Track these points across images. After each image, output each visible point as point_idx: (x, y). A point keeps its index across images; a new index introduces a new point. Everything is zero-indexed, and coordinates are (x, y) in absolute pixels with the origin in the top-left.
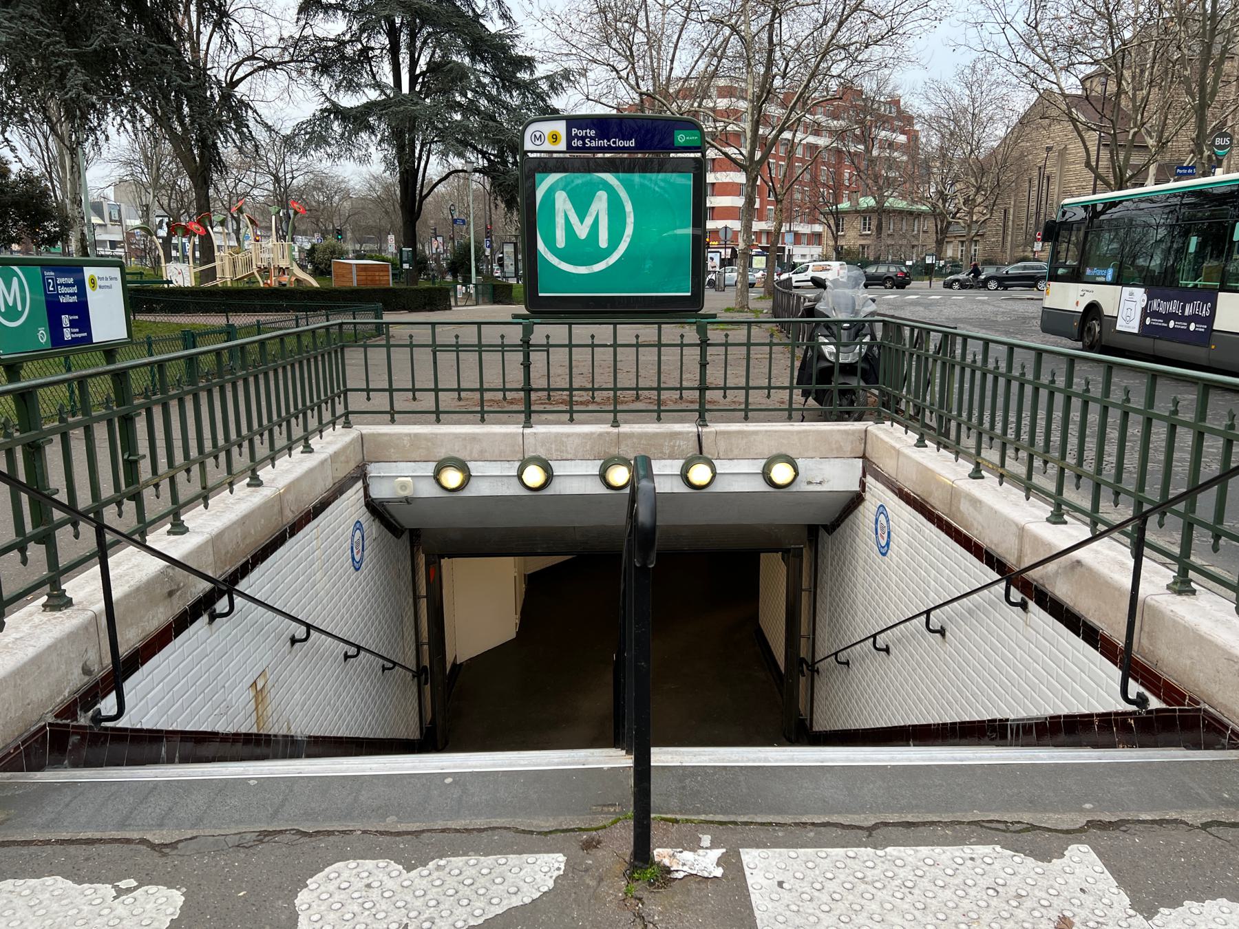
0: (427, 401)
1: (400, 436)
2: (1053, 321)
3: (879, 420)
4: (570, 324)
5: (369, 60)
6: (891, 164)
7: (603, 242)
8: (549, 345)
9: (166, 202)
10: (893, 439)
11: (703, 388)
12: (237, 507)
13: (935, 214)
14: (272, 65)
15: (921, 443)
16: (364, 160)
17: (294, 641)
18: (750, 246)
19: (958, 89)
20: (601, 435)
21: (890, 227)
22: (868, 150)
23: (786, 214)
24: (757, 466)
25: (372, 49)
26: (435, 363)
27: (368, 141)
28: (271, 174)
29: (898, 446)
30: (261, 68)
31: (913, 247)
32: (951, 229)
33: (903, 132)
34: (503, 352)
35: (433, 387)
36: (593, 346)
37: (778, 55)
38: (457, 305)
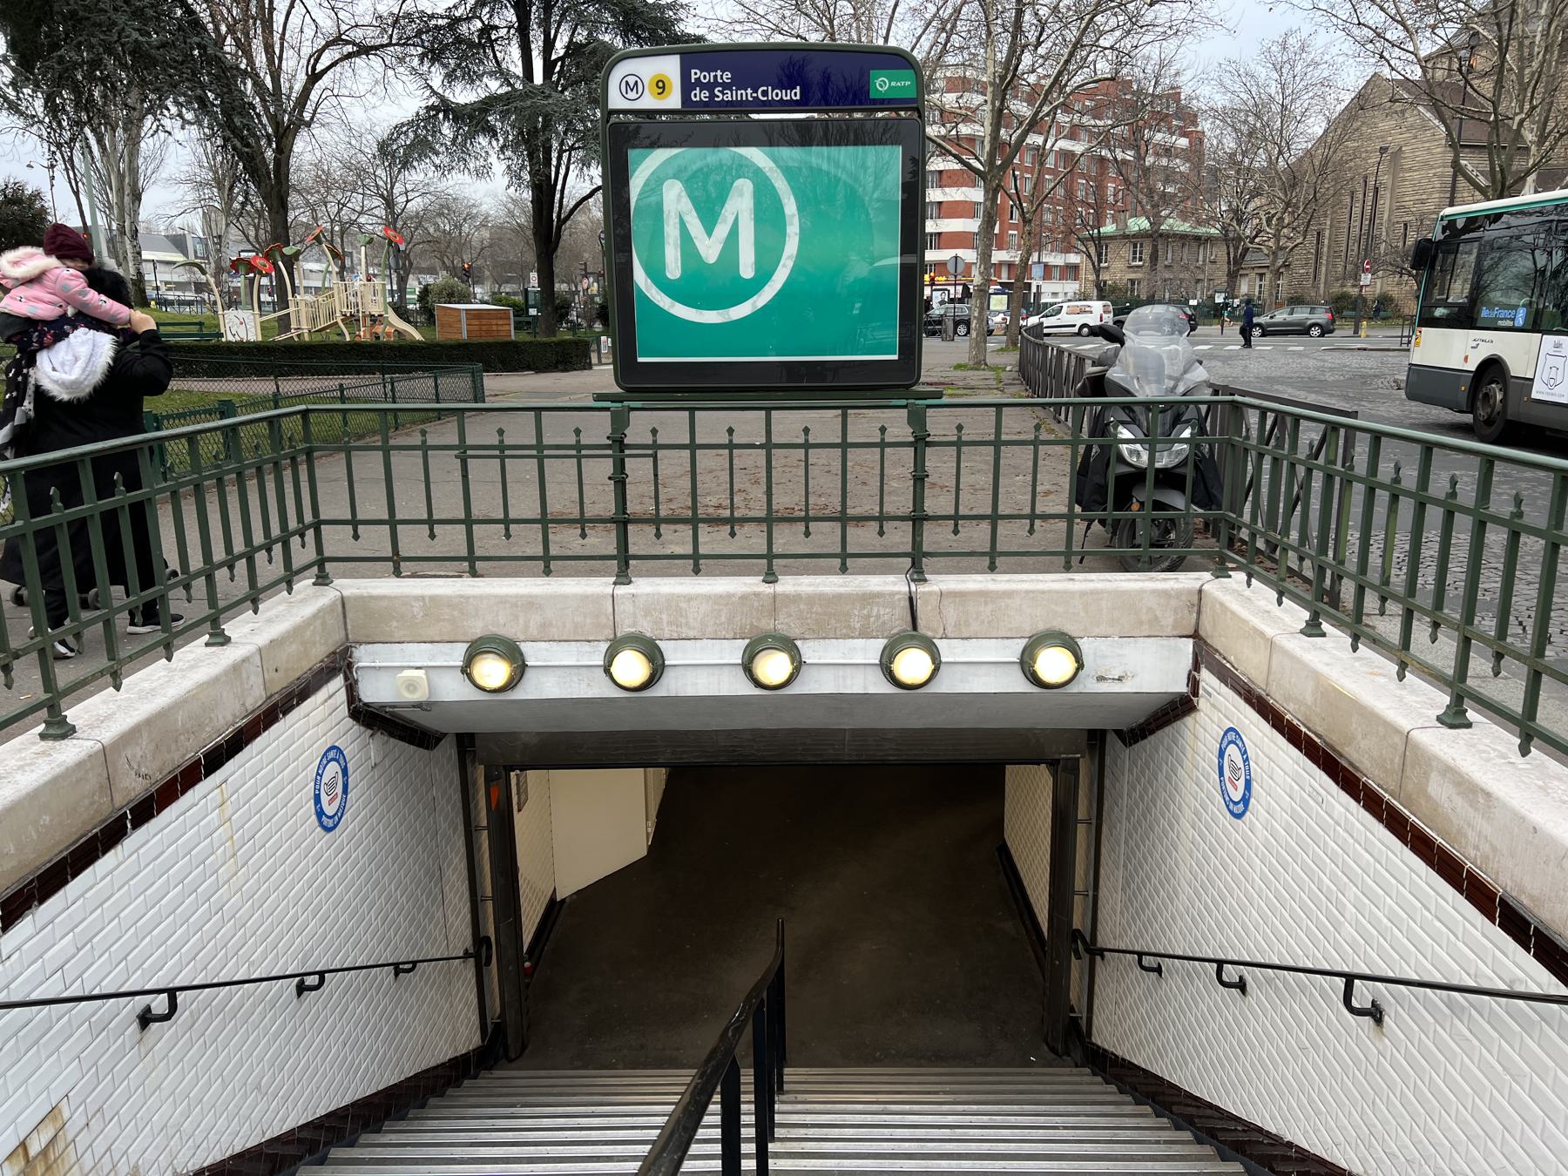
0: (452, 539)
1: (406, 600)
2: (1426, 384)
3: (1221, 572)
4: (692, 410)
5: (492, 42)
6: (1169, 176)
7: (747, 271)
8: (656, 446)
9: (252, 233)
10: (1254, 613)
11: (918, 519)
12: (18, 776)
13: (1226, 238)
14: (364, 50)
15: (1313, 629)
16: (483, 172)
17: (146, 1019)
18: (988, 282)
19: (1264, 73)
20: (744, 598)
21: (1168, 256)
22: (1140, 158)
23: (1033, 242)
25: (496, 28)
26: (465, 476)
27: (488, 148)
28: (382, 196)
29: (1270, 631)
30: (349, 56)
31: (1198, 281)
32: (1247, 258)
33: (1185, 135)
34: (579, 458)
35: (462, 516)
37: (1028, 17)
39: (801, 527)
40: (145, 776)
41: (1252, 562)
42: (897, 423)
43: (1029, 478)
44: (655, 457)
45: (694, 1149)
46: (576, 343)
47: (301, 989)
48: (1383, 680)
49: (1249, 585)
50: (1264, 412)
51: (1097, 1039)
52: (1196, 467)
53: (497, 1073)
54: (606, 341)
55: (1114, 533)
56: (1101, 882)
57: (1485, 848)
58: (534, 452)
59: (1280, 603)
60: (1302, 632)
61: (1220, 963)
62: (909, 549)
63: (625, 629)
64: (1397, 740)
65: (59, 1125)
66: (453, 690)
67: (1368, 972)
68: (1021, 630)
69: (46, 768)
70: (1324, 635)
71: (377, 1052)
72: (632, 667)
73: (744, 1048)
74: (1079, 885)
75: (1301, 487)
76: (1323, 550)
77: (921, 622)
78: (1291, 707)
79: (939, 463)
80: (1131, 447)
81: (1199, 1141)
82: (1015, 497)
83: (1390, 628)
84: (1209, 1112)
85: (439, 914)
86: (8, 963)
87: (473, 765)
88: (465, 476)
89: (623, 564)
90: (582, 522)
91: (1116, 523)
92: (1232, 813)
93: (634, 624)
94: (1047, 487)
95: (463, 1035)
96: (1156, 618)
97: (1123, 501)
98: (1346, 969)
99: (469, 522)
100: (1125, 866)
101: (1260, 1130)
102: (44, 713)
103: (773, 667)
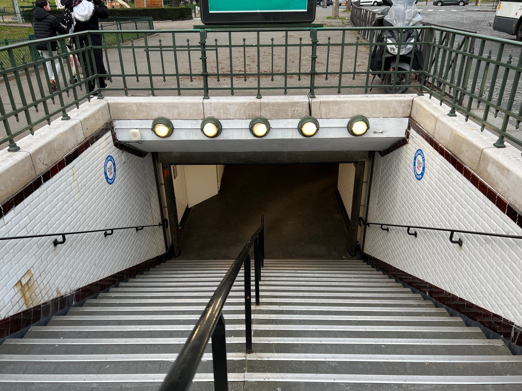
1: (130, 104)
3: (421, 94)
4: (230, 32)
8: (217, 46)
10: (431, 108)
15: (452, 114)
17: (56, 243)
20: (250, 104)
24: (345, 123)
26: (148, 58)
29: (436, 115)
34: (189, 51)
36: (244, 46)
38: (196, 17)
39: (270, 78)
40: (46, 165)
41: (432, 90)
42: (306, 36)
43: (353, 60)
44: (217, 50)
45: (237, 279)
46: (187, 9)
47: (106, 234)
48: (475, 131)
49: (430, 98)
50: (442, 32)
51: (365, 251)
52: (415, 54)
53: (171, 261)
54: (198, 8)
55: (383, 80)
56: (370, 202)
57: (506, 189)
58: (173, 49)
59: (441, 104)
60: (448, 115)
61: (409, 227)
62: (309, 86)
63: (207, 116)
64: (479, 152)
65: (31, 275)
66: (149, 137)
67: (459, 229)
68: (348, 116)
69: (12, 161)
70: (456, 116)
71: (132, 254)
72: (210, 129)
73: (251, 251)
74: (362, 203)
75: (453, 62)
76: (458, 84)
77: (313, 113)
78: (442, 141)
79: (321, 53)
80: (392, 48)
81: (397, 282)
82: (348, 66)
83: (480, 114)
84: (401, 273)
85: (150, 212)
86: (7, 225)
87: (158, 163)
88: (148, 58)
89: (206, 92)
90: (191, 76)
91: (384, 75)
92: (417, 178)
93: (211, 113)
94: (360, 63)
95: (160, 249)
96: (396, 110)
97: (387, 68)
98: (451, 229)
99: (150, 75)
100: (378, 196)
101: (417, 278)
102: (8, 143)
103: (260, 129)
